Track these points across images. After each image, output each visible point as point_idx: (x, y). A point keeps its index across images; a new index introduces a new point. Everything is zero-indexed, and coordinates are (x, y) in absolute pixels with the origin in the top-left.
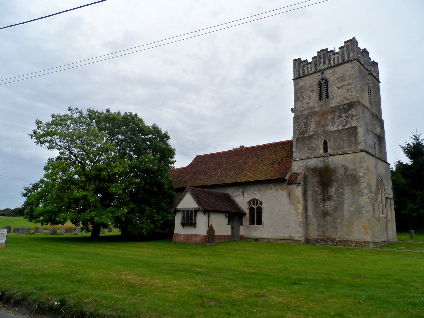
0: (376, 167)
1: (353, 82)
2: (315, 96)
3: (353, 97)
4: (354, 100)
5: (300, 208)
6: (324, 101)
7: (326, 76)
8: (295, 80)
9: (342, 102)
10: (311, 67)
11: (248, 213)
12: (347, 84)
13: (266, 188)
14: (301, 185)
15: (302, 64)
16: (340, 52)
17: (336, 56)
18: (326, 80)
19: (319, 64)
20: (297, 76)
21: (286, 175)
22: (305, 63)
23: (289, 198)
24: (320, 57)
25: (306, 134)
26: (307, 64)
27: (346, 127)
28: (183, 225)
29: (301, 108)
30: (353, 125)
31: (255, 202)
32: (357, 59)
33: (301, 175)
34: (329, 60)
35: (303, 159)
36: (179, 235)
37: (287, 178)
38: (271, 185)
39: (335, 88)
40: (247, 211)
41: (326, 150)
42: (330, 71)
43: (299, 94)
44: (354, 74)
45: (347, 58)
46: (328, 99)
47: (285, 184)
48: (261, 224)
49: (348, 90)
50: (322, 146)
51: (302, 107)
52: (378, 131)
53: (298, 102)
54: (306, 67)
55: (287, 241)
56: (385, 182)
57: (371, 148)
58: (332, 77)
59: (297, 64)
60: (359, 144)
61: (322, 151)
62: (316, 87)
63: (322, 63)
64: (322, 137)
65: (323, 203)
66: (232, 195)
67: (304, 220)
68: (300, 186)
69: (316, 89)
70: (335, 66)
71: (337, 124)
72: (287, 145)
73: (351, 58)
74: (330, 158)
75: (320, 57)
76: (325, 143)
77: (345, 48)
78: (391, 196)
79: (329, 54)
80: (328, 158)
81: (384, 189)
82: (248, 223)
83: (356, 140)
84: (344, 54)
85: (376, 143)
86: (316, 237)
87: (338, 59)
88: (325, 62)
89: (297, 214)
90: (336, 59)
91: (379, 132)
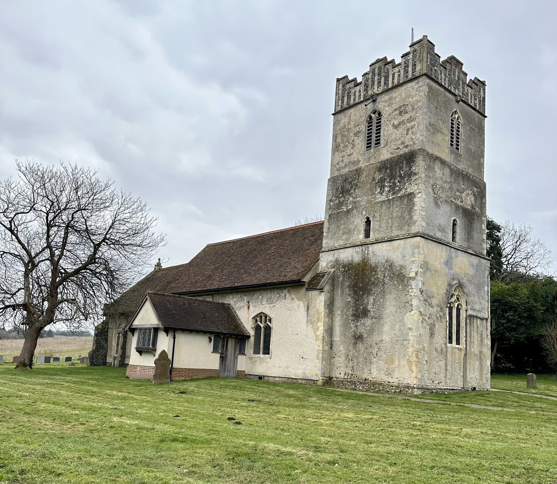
0: (448, 263)
1: (417, 115)
2: (360, 142)
3: (414, 142)
4: (416, 147)
5: (320, 328)
6: (372, 150)
7: (379, 106)
8: (336, 116)
9: (397, 151)
10: (360, 91)
11: (253, 336)
12: (408, 119)
13: (278, 295)
14: (323, 291)
15: (348, 86)
16: (404, 63)
17: (397, 69)
18: (380, 114)
19: (372, 85)
20: (339, 108)
21: (304, 276)
22: (352, 85)
23: (308, 312)
24: (374, 74)
25: (343, 207)
26: (355, 87)
27: (399, 195)
28: (140, 351)
29: (341, 163)
30: (409, 191)
31: (263, 318)
32: (425, 75)
33: (328, 274)
34: (387, 78)
35: (335, 250)
36: (135, 367)
37: (306, 279)
38: (286, 291)
39: (391, 127)
40: (252, 333)
41: (367, 235)
42: (385, 97)
43: (339, 140)
44: (420, 101)
45: (412, 73)
46: (379, 146)
47: (303, 290)
48: (268, 354)
49: (408, 130)
50: (362, 228)
51: (342, 161)
52: (468, 200)
53: (337, 153)
54: (353, 91)
55: (300, 381)
56: (470, 288)
57: (443, 230)
58: (387, 109)
59: (341, 86)
60: (414, 223)
61: (362, 236)
62: (363, 127)
63: (376, 83)
64: (364, 212)
65: (356, 321)
66: (234, 306)
67: (327, 348)
68: (322, 293)
69: (364, 130)
70: (395, 87)
71: (387, 189)
72: (319, 226)
73: (417, 74)
74: (371, 248)
75: (374, 74)
76: (368, 222)
77: (411, 56)
78: (486, 314)
79: (387, 66)
80: (368, 248)
81: (465, 301)
82: (252, 350)
83: (411, 218)
84: (407, 66)
85: (458, 222)
86: (342, 376)
87: (399, 75)
88: (380, 82)
89: (317, 336)
90: (396, 75)
91: (469, 202)
